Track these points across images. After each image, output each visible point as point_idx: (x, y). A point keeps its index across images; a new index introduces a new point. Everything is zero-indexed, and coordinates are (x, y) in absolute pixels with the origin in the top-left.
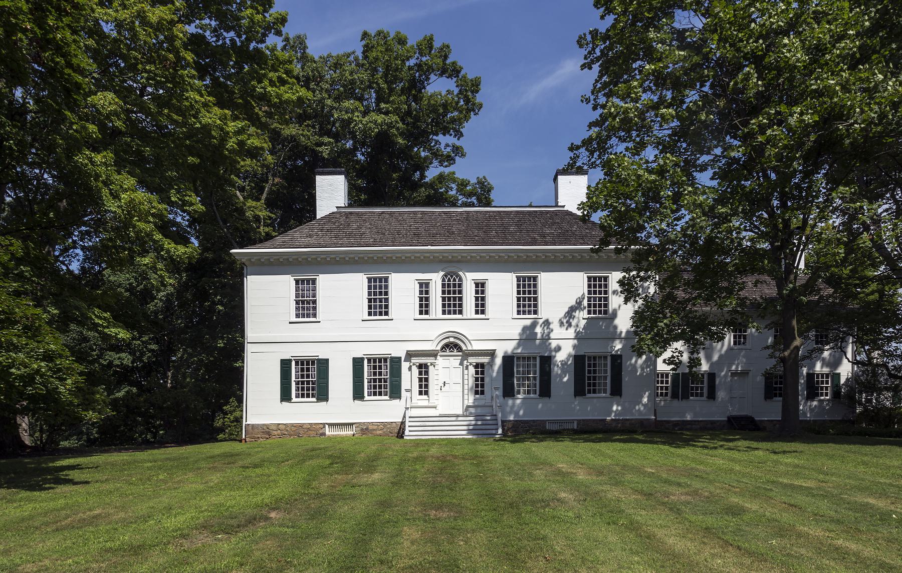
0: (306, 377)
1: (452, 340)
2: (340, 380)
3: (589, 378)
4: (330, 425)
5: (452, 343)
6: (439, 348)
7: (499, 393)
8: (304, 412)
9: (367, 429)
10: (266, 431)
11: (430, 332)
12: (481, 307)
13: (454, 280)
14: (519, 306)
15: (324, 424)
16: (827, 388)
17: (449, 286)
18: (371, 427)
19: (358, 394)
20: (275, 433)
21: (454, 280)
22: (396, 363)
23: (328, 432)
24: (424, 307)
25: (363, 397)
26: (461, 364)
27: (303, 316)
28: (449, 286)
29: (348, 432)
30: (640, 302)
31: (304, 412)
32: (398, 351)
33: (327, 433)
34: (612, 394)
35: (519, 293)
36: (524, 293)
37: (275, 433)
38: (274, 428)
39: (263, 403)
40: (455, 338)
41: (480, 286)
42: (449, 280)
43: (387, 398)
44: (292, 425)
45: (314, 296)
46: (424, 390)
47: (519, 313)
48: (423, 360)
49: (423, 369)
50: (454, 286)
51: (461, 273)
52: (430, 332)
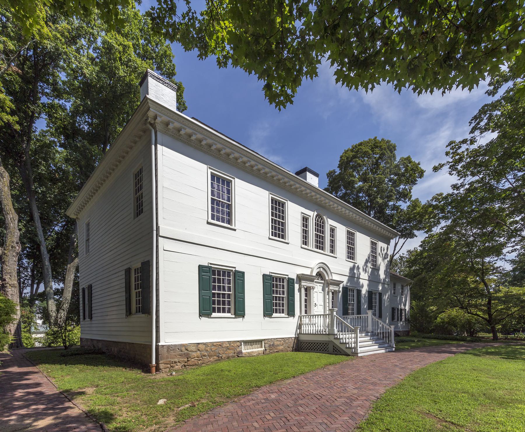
0: (219, 290)
2: (254, 295)
4: (247, 342)
8: (223, 329)
9: (273, 345)
10: (184, 351)
11: (310, 261)
15: (240, 342)
16: (229, 295)
18: (276, 343)
19: (268, 312)
20: (195, 354)
22: (291, 282)
23: (245, 350)
26: (323, 290)
27: (218, 220)
29: (257, 350)
30: (487, 260)
31: (223, 329)
32: (292, 273)
33: (243, 351)
37: (195, 354)
38: (194, 348)
39: (179, 321)
40: (323, 269)
41: (333, 230)
44: (213, 344)
45: (229, 199)
49: (308, 290)
51: (325, 217)
52: (310, 261)
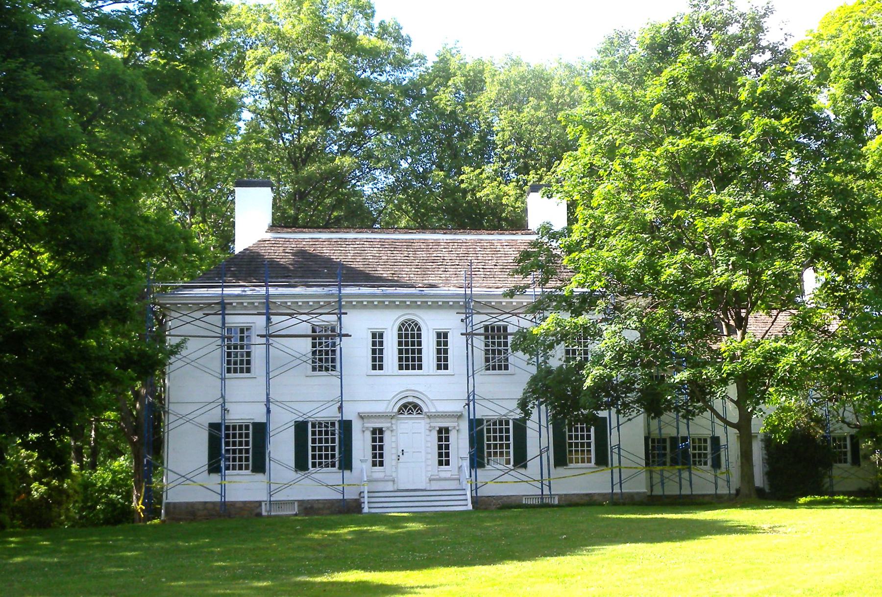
0: (236, 445)
1: (410, 400)
2: (281, 447)
3: (489, 446)
5: (410, 403)
6: (396, 410)
7: (466, 464)
9: (312, 508)
12: (442, 363)
13: (413, 330)
14: (400, 359)
17: (407, 336)
18: (315, 506)
19: (301, 464)
21: (413, 330)
24: (377, 363)
25: (307, 469)
28: (407, 336)
34: (340, 468)
35: (400, 343)
36: (407, 344)
42: (406, 330)
43: (248, 472)
46: (378, 459)
47: (401, 367)
48: (444, 424)
49: (378, 435)
50: (413, 336)
